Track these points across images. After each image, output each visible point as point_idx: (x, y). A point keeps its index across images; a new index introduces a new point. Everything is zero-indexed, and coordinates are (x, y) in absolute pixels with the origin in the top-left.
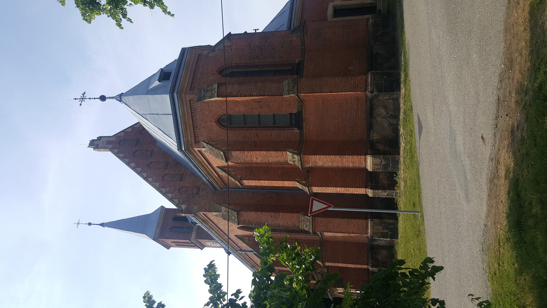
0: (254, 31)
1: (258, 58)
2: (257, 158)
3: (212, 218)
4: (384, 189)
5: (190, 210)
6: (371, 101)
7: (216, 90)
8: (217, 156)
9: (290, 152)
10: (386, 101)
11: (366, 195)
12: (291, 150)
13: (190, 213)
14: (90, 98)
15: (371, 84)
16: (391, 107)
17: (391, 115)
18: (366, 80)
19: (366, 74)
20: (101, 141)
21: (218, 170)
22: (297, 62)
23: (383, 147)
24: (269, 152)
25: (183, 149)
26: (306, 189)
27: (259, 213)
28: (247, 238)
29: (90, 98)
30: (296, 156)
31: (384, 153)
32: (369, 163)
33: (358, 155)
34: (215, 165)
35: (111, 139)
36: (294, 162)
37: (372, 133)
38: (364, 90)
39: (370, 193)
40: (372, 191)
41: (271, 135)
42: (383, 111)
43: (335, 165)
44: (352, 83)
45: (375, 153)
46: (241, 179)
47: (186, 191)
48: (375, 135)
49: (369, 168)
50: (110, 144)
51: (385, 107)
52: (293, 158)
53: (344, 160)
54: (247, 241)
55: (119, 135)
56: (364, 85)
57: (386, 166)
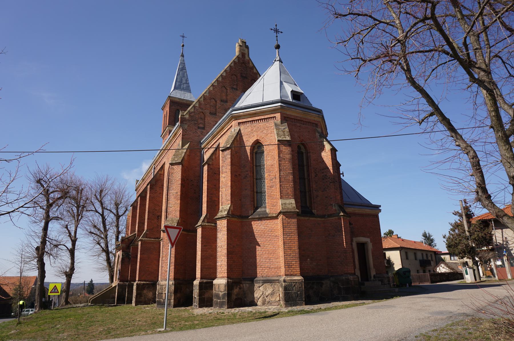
0: (341, 172)
1: (316, 176)
2: (224, 178)
3: (177, 141)
4: (200, 295)
5: (184, 122)
6: (278, 280)
7: (284, 139)
8: (227, 142)
9: (230, 207)
10: (278, 294)
11: (195, 279)
12: (232, 208)
13: (181, 123)
14: (277, 37)
15: (292, 280)
16: (273, 299)
17: (265, 300)
18: (296, 275)
19: (301, 275)
20: (245, 48)
21: (217, 144)
22: (313, 211)
23: (235, 293)
24: (230, 188)
25: (233, 112)
26: (199, 223)
27: (180, 182)
28: (162, 173)
29: (277, 37)
30: (226, 213)
31: (229, 294)
32: (220, 282)
33: (227, 270)
34: (221, 141)
35: (246, 56)
36: (222, 211)
37: (249, 282)
38: (287, 273)
39: (196, 283)
40: (198, 283)
41: (246, 190)
42: (269, 291)
43: (219, 249)
44: (293, 262)
45: (230, 286)
46: (208, 165)
47: (201, 118)
48: (247, 285)
49: (215, 282)
50: (242, 56)
51: (272, 294)
52: (225, 210)
53: (223, 258)
54: (160, 173)
55: (250, 63)
56: (291, 273)
57: (218, 296)
